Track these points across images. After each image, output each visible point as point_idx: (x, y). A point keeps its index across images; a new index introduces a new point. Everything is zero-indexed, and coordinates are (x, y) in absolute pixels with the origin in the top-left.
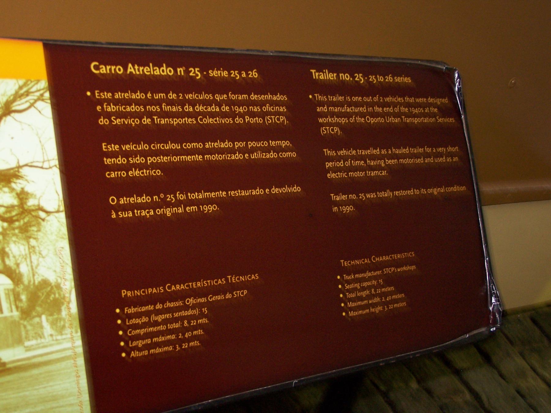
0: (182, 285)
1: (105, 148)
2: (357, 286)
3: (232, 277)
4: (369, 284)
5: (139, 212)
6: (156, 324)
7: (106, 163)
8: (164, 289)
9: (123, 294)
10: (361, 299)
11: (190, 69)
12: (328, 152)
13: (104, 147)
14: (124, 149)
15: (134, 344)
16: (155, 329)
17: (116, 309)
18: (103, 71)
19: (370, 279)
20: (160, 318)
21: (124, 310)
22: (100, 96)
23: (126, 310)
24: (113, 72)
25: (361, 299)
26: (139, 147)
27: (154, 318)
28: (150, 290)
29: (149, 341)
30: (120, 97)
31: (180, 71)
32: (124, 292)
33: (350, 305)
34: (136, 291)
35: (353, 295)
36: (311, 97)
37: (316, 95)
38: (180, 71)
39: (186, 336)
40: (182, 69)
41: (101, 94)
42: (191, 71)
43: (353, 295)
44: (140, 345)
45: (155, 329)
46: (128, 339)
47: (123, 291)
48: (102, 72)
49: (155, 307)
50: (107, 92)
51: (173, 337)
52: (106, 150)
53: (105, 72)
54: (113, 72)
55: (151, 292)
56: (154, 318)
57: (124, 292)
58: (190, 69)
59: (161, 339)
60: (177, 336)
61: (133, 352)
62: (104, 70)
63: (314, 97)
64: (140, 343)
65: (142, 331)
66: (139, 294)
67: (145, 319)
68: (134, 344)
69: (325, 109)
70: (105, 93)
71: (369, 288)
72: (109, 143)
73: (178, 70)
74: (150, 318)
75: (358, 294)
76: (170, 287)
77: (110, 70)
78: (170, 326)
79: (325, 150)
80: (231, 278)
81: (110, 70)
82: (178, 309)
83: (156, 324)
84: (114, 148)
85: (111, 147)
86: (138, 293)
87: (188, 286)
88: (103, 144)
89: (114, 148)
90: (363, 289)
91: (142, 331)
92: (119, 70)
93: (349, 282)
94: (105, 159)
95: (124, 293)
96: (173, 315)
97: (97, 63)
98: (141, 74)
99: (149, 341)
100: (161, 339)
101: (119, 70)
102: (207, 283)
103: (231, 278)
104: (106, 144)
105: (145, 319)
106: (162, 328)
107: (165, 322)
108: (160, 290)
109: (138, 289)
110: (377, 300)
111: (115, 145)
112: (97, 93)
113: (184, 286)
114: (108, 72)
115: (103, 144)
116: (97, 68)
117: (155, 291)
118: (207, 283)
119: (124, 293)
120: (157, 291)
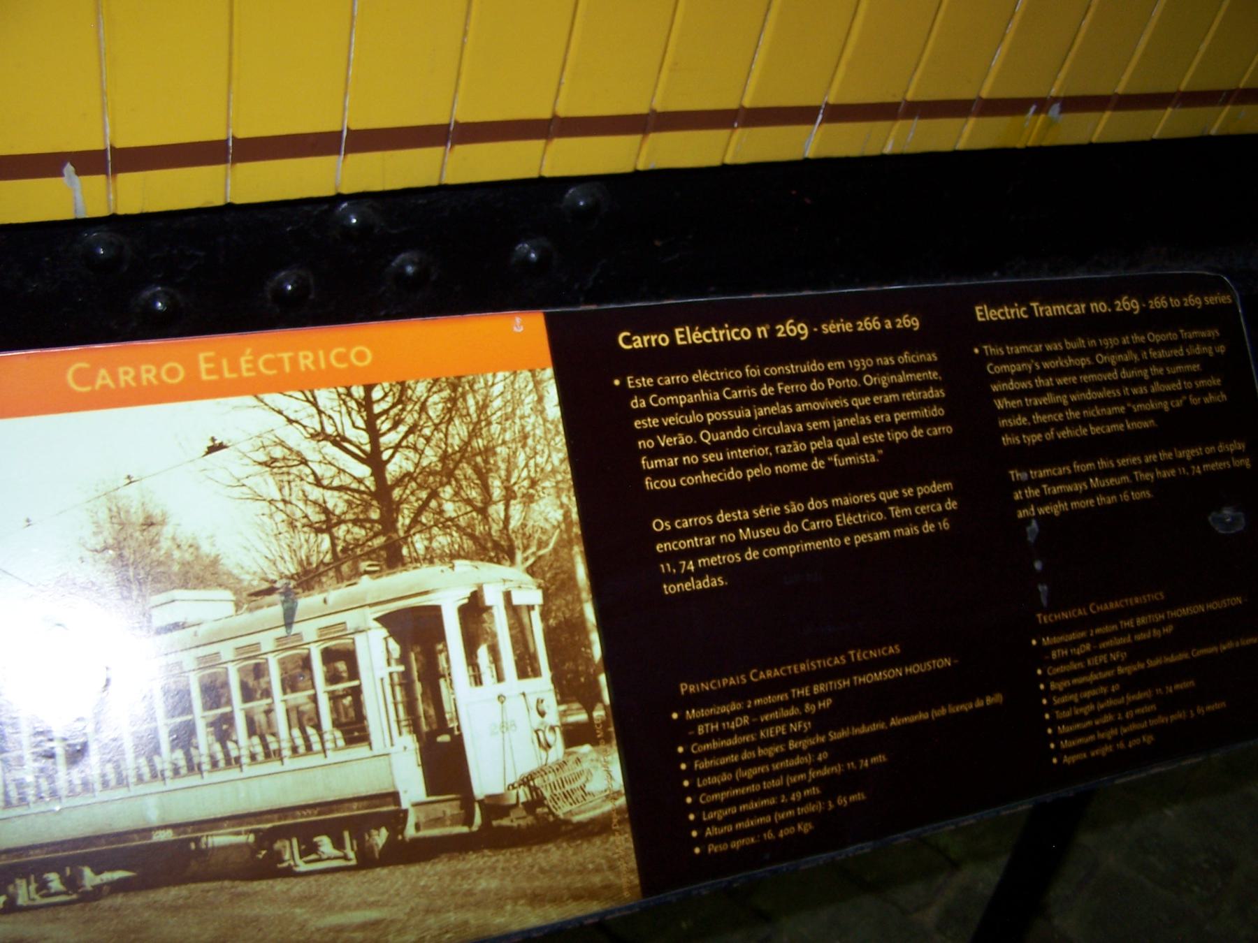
0: (776, 670)
1: (632, 384)
2: (1074, 697)
3: (857, 651)
4: (1094, 692)
5: (701, 540)
6: (745, 782)
7: (667, 593)
8: (748, 677)
9: (682, 690)
10: (1081, 718)
11: (778, 327)
12: (1015, 475)
13: (629, 382)
14: (666, 424)
15: (711, 816)
16: (743, 791)
17: (695, 847)
18: (638, 344)
19: (1096, 684)
20: (750, 773)
21: (693, 765)
22: (634, 384)
23: (696, 766)
24: (654, 344)
25: (1081, 718)
26: (689, 420)
27: (740, 774)
28: (725, 681)
29: (734, 810)
30: (697, 545)
31: (762, 332)
32: (684, 687)
33: (1063, 729)
34: (702, 685)
35: (1067, 714)
36: (976, 351)
37: (985, 347)
38: (762, 332)
39: (793, 798)
40: (764, 328)
41: (637, 381)
42: (780, 329)
43: (1067, 714)
44: (720, 818)
45: (743, 791)
46: (700, 825)
47: (682, 685)
48: (636, 347)
49: (740, 757)
50: (652, 418)
51: (772, 801)
52: (633, 387)
53: (641, 346)
54: (654, 344)
55: (727, 685)
56: (740, 774)
57: (684, 687)
58: (778, 327)
59: (753, 805)
60: (779, 800)
61: (708, 829)
62: (639, 342)
63: (982, 351)
64: (720, 814)
65: (722, 796)
66: (707, 688)
67: (726, 777)
68: (711, 816)
69: (999, 369)
70: (643, 379)
71: (1094, 700)
72: (638, 376)
73: (759, 330)
74: (734, 774)
75: (1077, 712)
76: (756, 675)
77: (649, 341)
78: (766, 785)
79: (1012, 472)
80: (855, 655)
81: (649, 341)
82: (779, 757)
83: (745, 782)
84: (646, 383)
85: (641, 382)
86: (705, 686)
87: (786, 671)
88: (629, 378)
89: (646, 383)
90: (1083, 702)
91: (722, 796)
92: (663, 340)
93: (1058, 693)
94: (665, 587)
95: (683, 688)
96: (771, 768)
97: (628, 334)
98: (769, 668)
99: (734, 810)
100: (753, 805)
101: (663, 340)
102: (816, 664)
103: (855, 655)
104: (632, 377)
105: (726, 777)
106: (753, 788)
107: (758, 779)
108: (741, 680)
109: (707, 679)
110: (1108, 718)
111: (646, 378)
112: (631, 380)
113: (779, 671)
114: (646, 345)
115: (629, 378)
116: (628, 340)
117: (732, 682)
118: (816, 664)
119: (683, 688)
120: (736, 681)
